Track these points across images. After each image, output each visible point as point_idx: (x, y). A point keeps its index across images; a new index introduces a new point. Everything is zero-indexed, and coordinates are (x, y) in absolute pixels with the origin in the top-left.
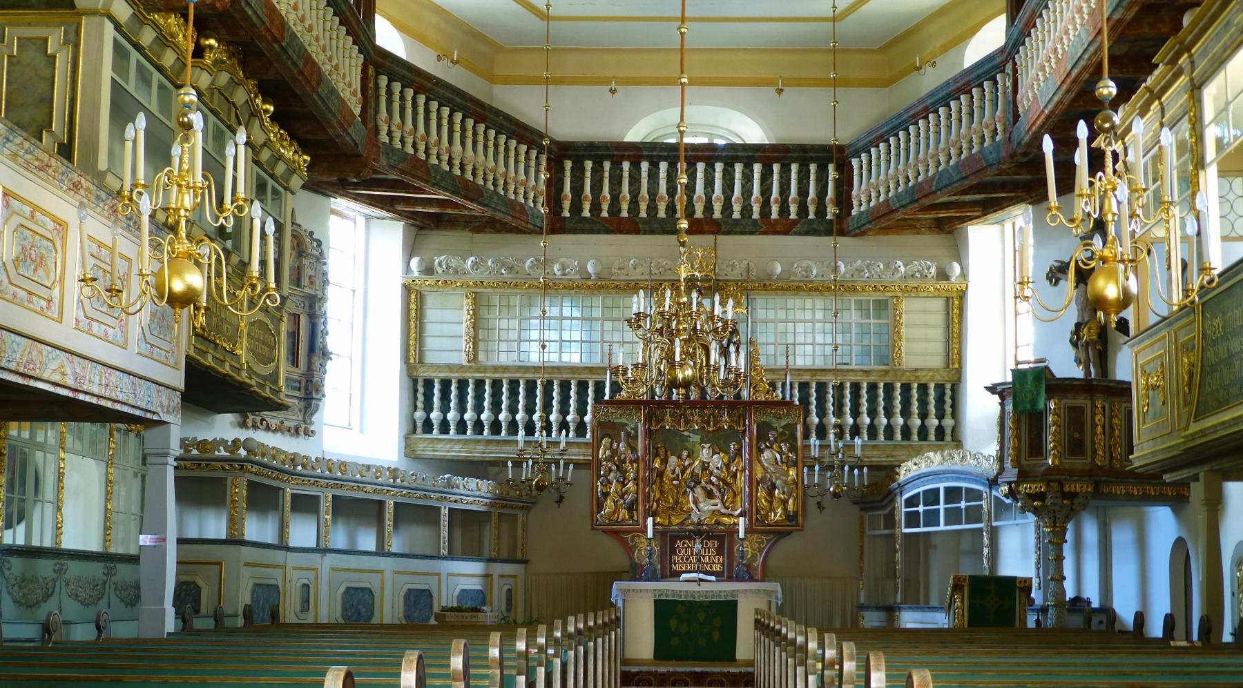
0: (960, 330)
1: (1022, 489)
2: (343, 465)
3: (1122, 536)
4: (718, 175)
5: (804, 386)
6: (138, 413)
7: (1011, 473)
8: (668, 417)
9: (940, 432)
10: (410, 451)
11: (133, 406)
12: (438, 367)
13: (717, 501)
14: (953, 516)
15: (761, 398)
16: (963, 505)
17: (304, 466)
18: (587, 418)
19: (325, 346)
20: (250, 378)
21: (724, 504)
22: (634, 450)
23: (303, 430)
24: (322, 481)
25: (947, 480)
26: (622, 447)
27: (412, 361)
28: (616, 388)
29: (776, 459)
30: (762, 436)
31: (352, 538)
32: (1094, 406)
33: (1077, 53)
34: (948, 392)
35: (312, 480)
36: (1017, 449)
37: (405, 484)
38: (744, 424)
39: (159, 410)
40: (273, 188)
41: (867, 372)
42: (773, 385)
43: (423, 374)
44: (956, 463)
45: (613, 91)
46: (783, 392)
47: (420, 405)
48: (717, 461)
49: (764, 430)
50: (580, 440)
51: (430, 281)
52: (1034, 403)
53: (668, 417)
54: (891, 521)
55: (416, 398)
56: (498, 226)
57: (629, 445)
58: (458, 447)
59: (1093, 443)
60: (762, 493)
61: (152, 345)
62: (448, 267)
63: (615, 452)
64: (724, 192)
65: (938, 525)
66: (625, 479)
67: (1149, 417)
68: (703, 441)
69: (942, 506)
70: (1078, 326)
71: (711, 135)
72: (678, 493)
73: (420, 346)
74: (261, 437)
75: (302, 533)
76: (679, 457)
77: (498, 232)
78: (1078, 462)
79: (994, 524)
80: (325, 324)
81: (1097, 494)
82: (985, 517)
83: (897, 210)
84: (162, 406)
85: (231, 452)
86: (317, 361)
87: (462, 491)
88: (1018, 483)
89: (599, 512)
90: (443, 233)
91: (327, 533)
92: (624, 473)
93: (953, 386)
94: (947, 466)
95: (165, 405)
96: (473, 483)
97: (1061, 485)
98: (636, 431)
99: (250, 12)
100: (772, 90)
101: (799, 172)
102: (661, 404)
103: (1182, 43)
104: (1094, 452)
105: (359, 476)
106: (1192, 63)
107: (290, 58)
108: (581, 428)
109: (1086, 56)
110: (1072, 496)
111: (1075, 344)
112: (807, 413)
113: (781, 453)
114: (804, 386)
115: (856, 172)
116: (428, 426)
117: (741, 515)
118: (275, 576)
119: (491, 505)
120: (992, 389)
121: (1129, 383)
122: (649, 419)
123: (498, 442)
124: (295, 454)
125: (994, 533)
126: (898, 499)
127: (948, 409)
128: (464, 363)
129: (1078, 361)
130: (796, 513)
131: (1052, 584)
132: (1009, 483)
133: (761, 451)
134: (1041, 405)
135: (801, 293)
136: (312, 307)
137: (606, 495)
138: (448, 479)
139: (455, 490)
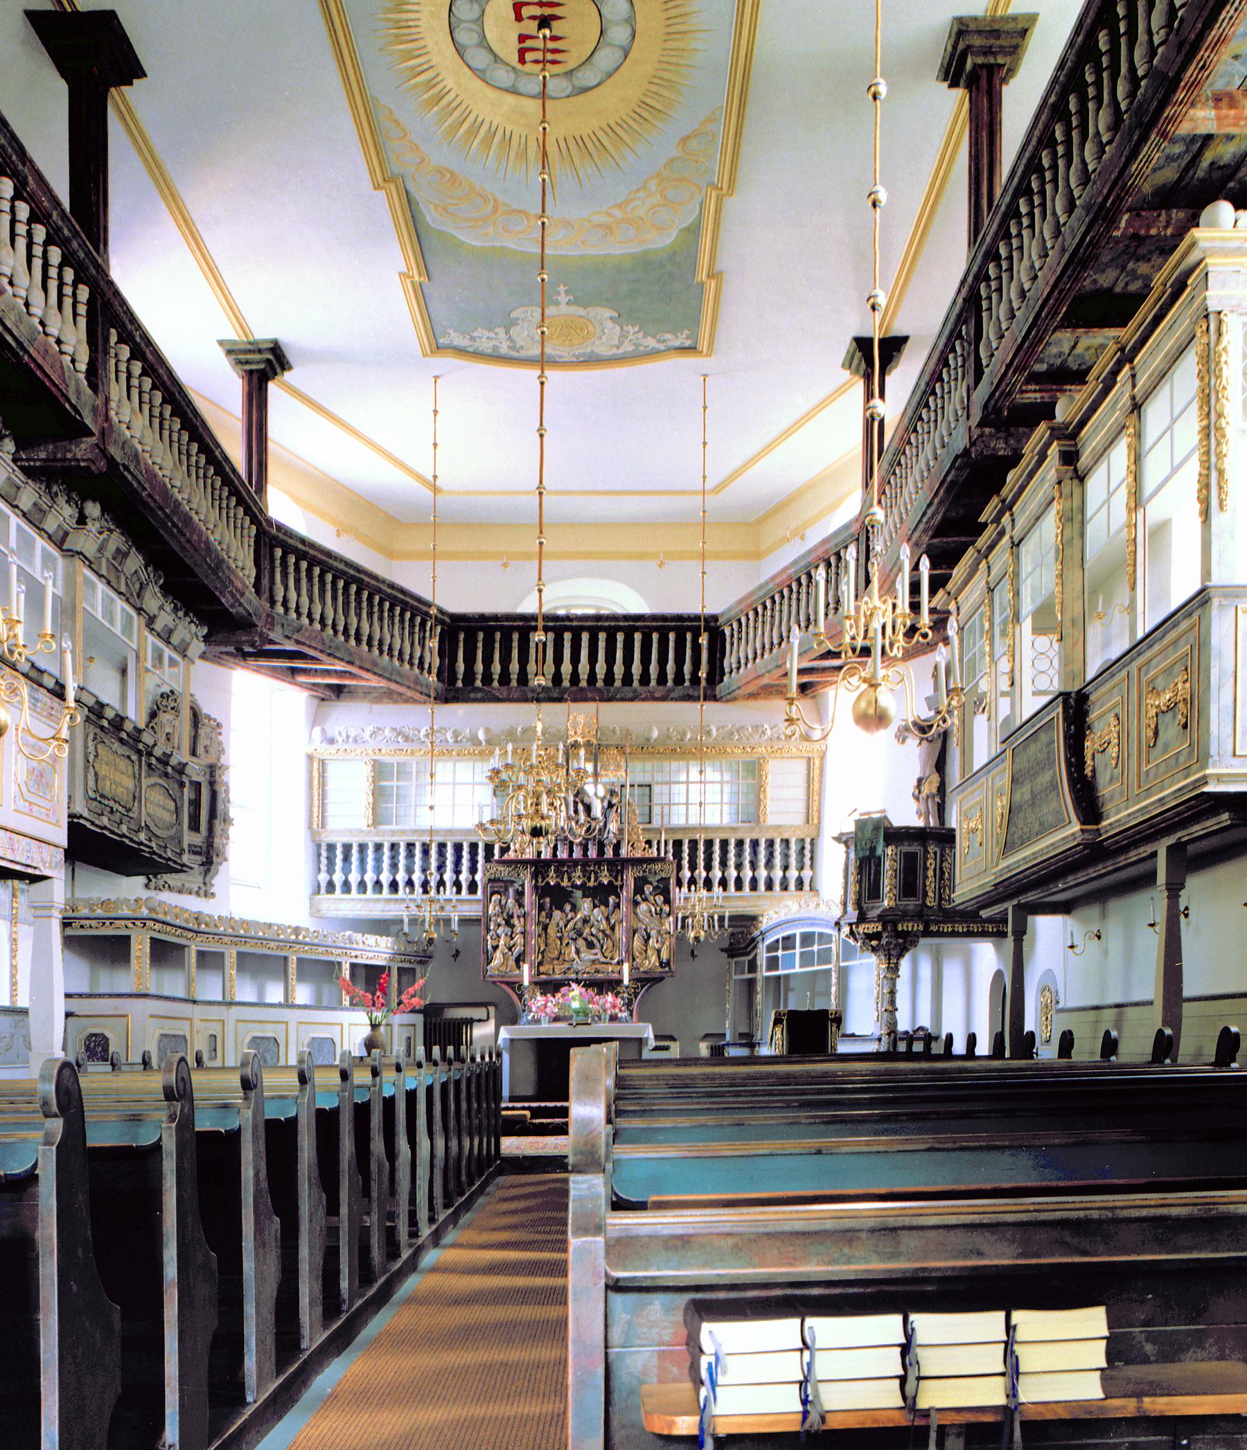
0: (820, 788)
1: (861, 930)
2: (244, 923)
3: (952, 973)
4: (602, 645)
5: (678, 844)
6: (18, 868)
7: (853, 914)
8: (552, 873)
9: (800, 883)
10: (315, 912)
11: (12, 861)
12: (339, 832)
14: (807, 959)
15: (638, 854)
16: (815, 948)
17: (206, 925)
18: (478, 877)
19: (226, 813)
20: (150, 840)
22: (521, 905)
23: (205, 892)
24: (226, 939)
25: (803, 925)
26: (511, 901)
27: (315, 826)
28: (504, 850)
30: (639, 890)
31: (261, 993)
32: (926, 852)
34: (808, 846)
35: (217, 938)
36: (860, 893)
37: (307, 940)
39: (40, 865)
40: (171, 659)
41: (734, 829)
42: (649, 842)
43: (327, 838)
44: (811, 912)
45: (505, 565)
46: (658, 849)
47: (323, 867)
48: (598, 914)
49: (640, 884)
50: (472, 897)
51: (332, 749)
52: (873, 849)
53: (552, 873)
54: (753, 967)
55: (319, 862)
56: (395, 696)
57: (517, 901)
58: (359, 906)
59: (925, 886)
60: (637, 942)
61: (31, 803)
62: (348, 737)
64: (606, 661)
65: (794, 967)
67: (970, 857)
68: (585, 896)
69: (798, 950)
70: (920, 781)
71: (598, 608)
73: (323, 812)
74: (167, 897)
75: (210, 988)
76: (562, 911)
77: (396, 702)
78: (911, 904)
79: (842, 964)
80: (227, 792)
81: (927, 933)
82: (834, 958)
83: (762, 675)
84: (44, 863)
85: (134, 910)
86: (218, 824)
87: (361, 946)
88: (857, 924)
89: (489, 963)
90: (344, 704)
91: (232, 987)
93: (812, 840)
94: (803, 914)
95: (50, 862)
96: (371, 939)
97: (895, 926)
99: (129, 477)
100: (653, 564)
101: (677, 641)
102: (547, 863)
103: (1003, 501)
104: (925, 894)
106: (1013, 521)
107: (174, 525)
108: (473, 887)
109: (925, 520)
110: (905, 935)
111: (917, 799)
112: (680, 867)
114: (678, 844)
115: (728, 640)
116: (331, 886)
118: (182, 1028)
119: (391, 960)
120: (838, 839)
121: (954, 830)
122: (535, 876)
123: (396, 900)
124: (199, 913)
125: (843, 974)
126: (760, 945)
127: (807, 861)
128: (364, 827)
129: (919, 813)
130: (669, 961)
131: (886, 1015)
132: (851, 925)
133: (636, 904)
134: (879, 852)
136: (212, 775)
137: (495, 948)
138: (350, 937)
139: (355, 946)
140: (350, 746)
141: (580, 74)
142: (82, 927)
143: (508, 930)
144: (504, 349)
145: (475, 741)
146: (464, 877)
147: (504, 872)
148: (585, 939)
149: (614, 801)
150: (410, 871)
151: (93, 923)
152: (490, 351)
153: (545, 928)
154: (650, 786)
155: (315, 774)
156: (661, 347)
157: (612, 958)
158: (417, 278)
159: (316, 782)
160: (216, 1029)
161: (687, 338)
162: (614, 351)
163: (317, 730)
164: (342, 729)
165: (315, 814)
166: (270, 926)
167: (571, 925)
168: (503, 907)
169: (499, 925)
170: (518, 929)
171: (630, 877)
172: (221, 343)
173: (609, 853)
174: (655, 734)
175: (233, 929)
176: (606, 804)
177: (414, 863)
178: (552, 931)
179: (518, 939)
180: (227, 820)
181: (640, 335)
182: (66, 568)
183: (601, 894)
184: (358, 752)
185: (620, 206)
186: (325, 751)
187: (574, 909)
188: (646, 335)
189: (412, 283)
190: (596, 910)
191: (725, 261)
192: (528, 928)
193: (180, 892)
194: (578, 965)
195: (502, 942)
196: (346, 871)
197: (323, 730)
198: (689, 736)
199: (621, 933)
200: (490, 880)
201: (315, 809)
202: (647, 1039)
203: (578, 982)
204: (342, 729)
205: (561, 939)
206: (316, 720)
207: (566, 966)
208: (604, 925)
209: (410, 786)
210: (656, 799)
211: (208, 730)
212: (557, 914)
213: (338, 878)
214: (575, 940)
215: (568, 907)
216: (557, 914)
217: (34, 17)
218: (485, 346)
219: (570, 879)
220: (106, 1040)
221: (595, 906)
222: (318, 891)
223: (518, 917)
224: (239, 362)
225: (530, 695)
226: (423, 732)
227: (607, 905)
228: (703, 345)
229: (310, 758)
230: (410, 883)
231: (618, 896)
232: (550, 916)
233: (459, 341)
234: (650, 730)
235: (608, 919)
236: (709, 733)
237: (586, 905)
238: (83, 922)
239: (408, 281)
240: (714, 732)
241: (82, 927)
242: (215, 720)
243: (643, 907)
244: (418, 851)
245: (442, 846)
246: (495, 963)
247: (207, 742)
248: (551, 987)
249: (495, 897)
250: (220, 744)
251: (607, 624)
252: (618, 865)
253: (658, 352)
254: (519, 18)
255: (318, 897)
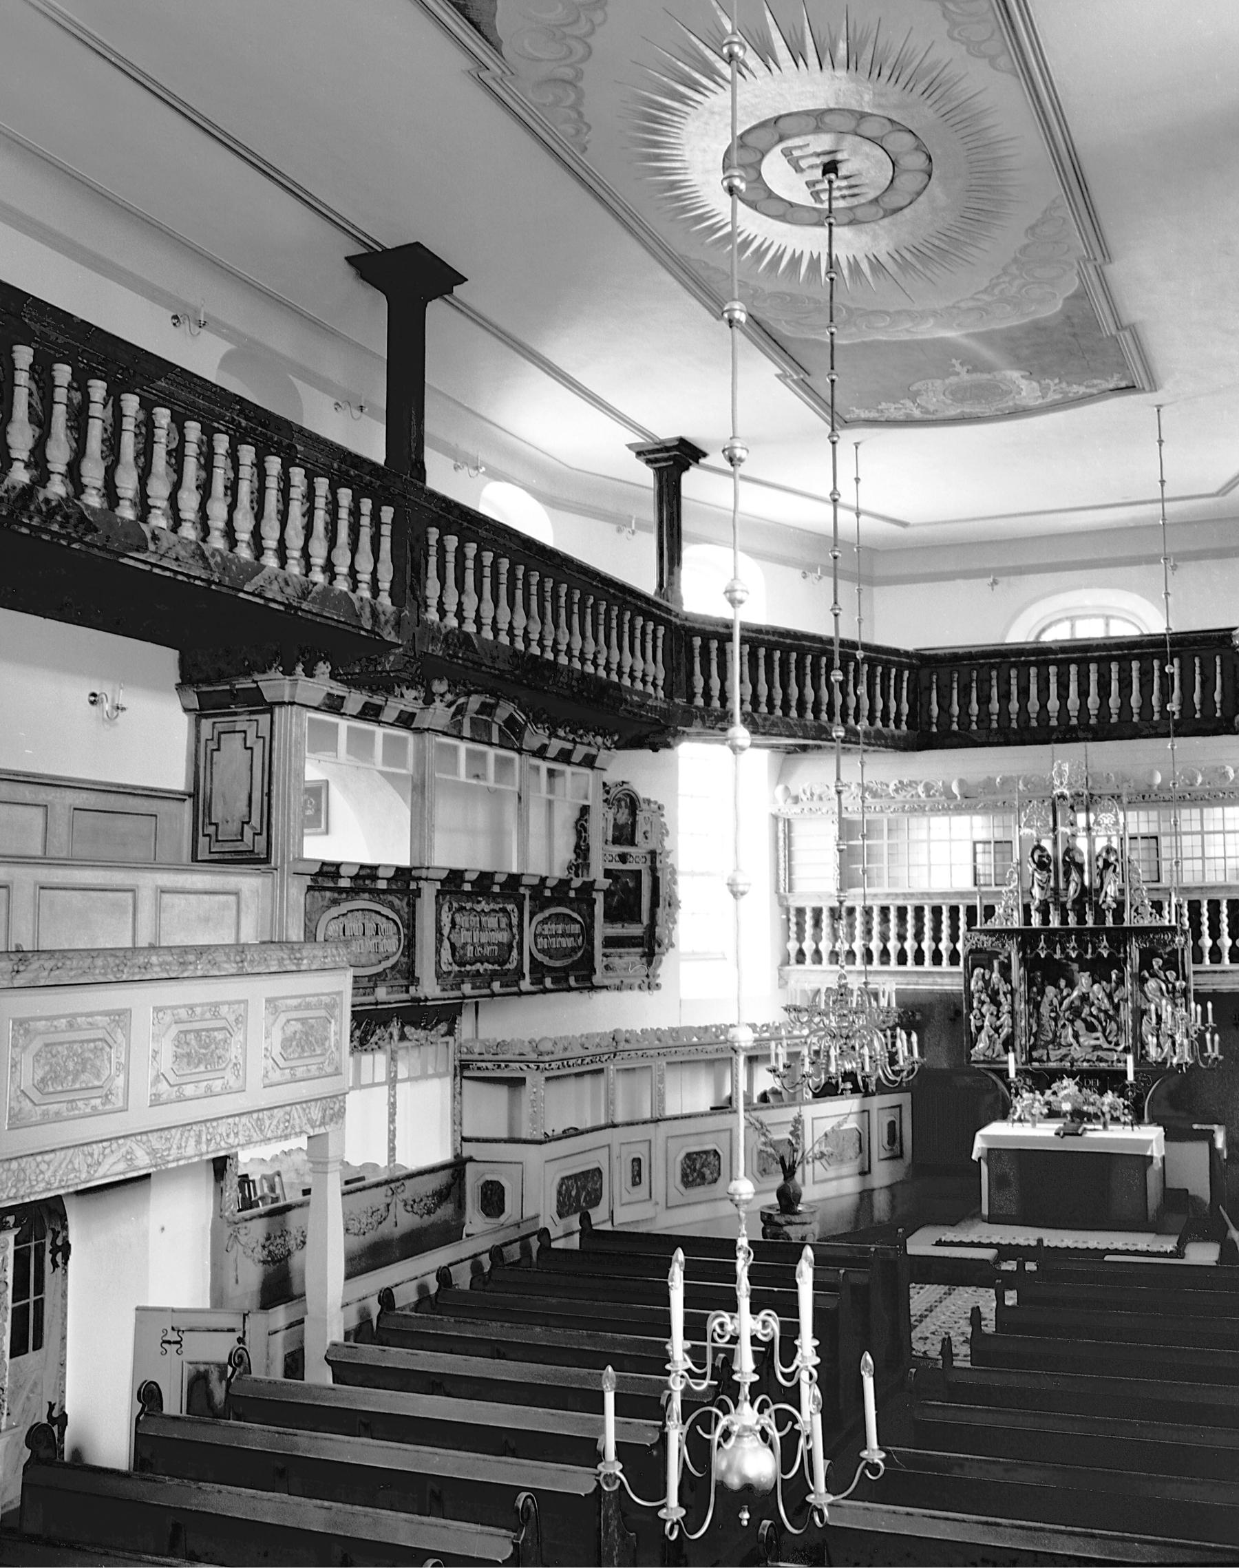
5: (1195, 907)
13: (1099, 1034)
18: (959, 946)
21: (1106, 1038)
22: (1008, 980)
24: (652, 1052)
26: (996, 975)
27: (782, 891)
29: (1161, 989)
30: (1145, 964)
33: (309, 1451)
35: (640, 1053)
38: (1125, 951)
43: (795, 903)
47: (793, 935)
51: (796, 809)
53: (1042, 944)
57: (1002, 975)
62: (812, 795)
63: (987, 983)
66: (998, 1011)
68: (1082, 970)
72: (1056, 1025)
73: (790, 874)
76: (1057, 986)
86: (661, 913)
92: (998, 1004)
98: (1010, 961)
105: (695, 1039)
108: (954, 958)
112: (1197, 935)
113: (1167, 981)
117: (1126, 1050)
122: (1021, 947)
133: (1143, 981)
135: (1185, 804)
136: (653, 860)
137: (980, 1029)
140: (816, 804)
141: (886, 199)
142: (479, 1068)
143: (993, 1009)
144: (917, 414)
145: (950, 796)
146: (944, 946)
147: (987, 942)
148: (1084, 1020)
149: (1112, 859)
150: (884, 938)
151: (490, 1065)
152: (902, 418)
153: (1037, 1006)
154: (1156, 838)
155: (781, 835)
156: (1094, 391)
157: (1117, 1044)
158: (795, 377)
159: (781, 843)
160: (640, 1151)
161: (1121, 379)
162: (1040, 401)
163: (781, 787)
164: (806, 785)
165: (782, 878)
166: (706, 1029)
167: (1066, 1002)
168: (987, 983)
169: (982, 1003)
170: (1005, 1008)
171: (1134, 951)
172: (630, 446)
173: (1109, 922)
174: (1158, 779)
175: (659, 1040)
176: (1101, 863)
177: (888, 929)
178: (1045, 1009)
179: (1005, 1019)
180: (673, 904)
181: (1064, 385)
182: (416, 745)
183: (1099, 970)
184: (824, 810)
185: (985, 291)
186: (790, 810)
187: (1071, 985)
188: (1069, 384)
189: (793, 381)
190: (1096, 987)
191: (1133, 312)
192: (1016, 1006)
193: (618, 989)
194: (1077, 1052)
195: (987, 1023)
196: (817, 939)
197: (787, 788)
198: (1200, 780)
199: (1126, 1015)
200: (971, 951)
201: (781, 872)
202: (1151, 1157)
203: (1072, 1075)
204: (806, 785)
205: (1056, 1019)
206: (782, 775)
207: (1063, 1051)
208: (1106, 1004)
209: (881, 843)
210: (1165, 853)
211: (647, 815)
212: (1050, 990)
213: (808, 946)
214: (1072, 1022)
215: (1063, 983)
216: (1050, 990)
217: (347, 258)
218: (900, 415)
219: (1063, 950)
220: (502, 1189)
221: (1094, 982)
222: (786, 962)
223: (1005, 994)
224: (648, 462)
225: (1012, 737)
226: (892, 787)
227: (1109, 981)
228: (1140, 379)
229: (775, 818)
230: (885, 953)
231: (1121, 971)
232: (1042, 993)
233: (864, 414)
234: (1152, 775)
235: (1110, 996)
236: (1225, 775)
237: (1084, 979)
238: (480, 1064)
239: (789, 381)
240: (1232, 775)
241: (479, 1068)
242: (656, 803)
243: (1152, 984)
244: (893, 915)
245: (919, 910)
246: (981, 1046)
247: (648, 828)
248: (1042, 1080)
249: (978, 971)
250: (663, 825)
251: (1096, 654)
252: (1120, 936)
253: (1091, 395)
254: (799, 170)
255: (787, 968)
